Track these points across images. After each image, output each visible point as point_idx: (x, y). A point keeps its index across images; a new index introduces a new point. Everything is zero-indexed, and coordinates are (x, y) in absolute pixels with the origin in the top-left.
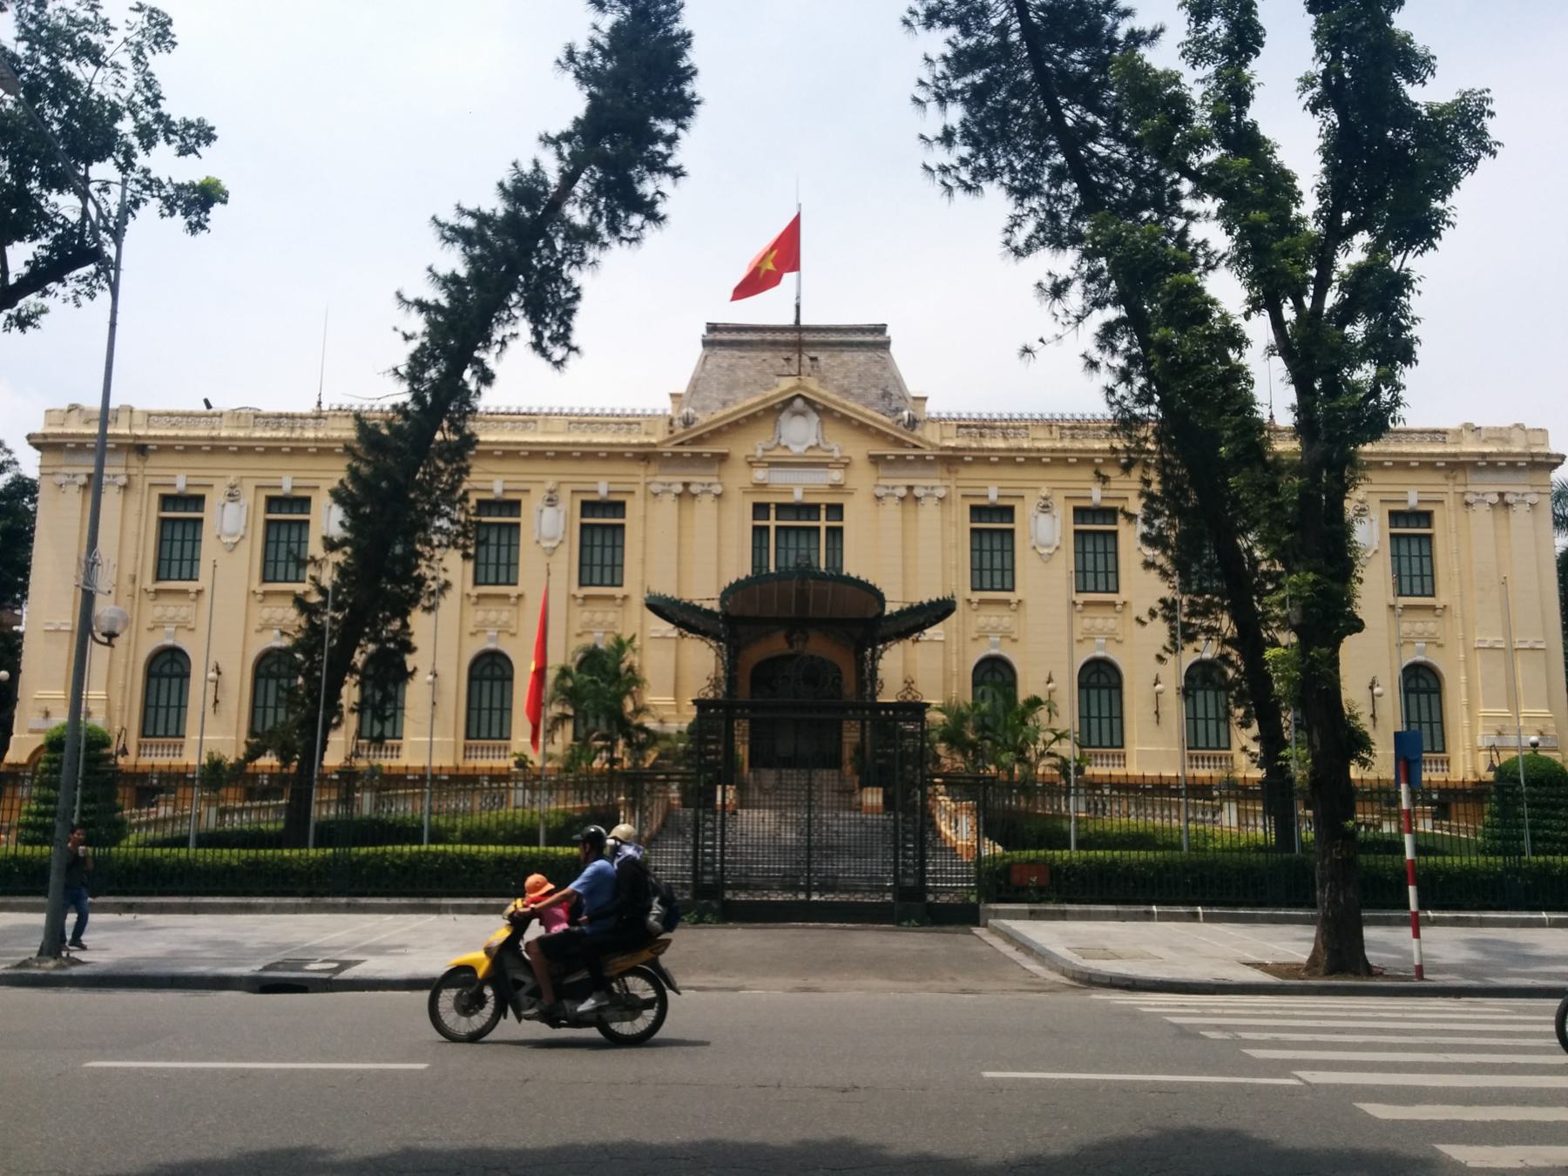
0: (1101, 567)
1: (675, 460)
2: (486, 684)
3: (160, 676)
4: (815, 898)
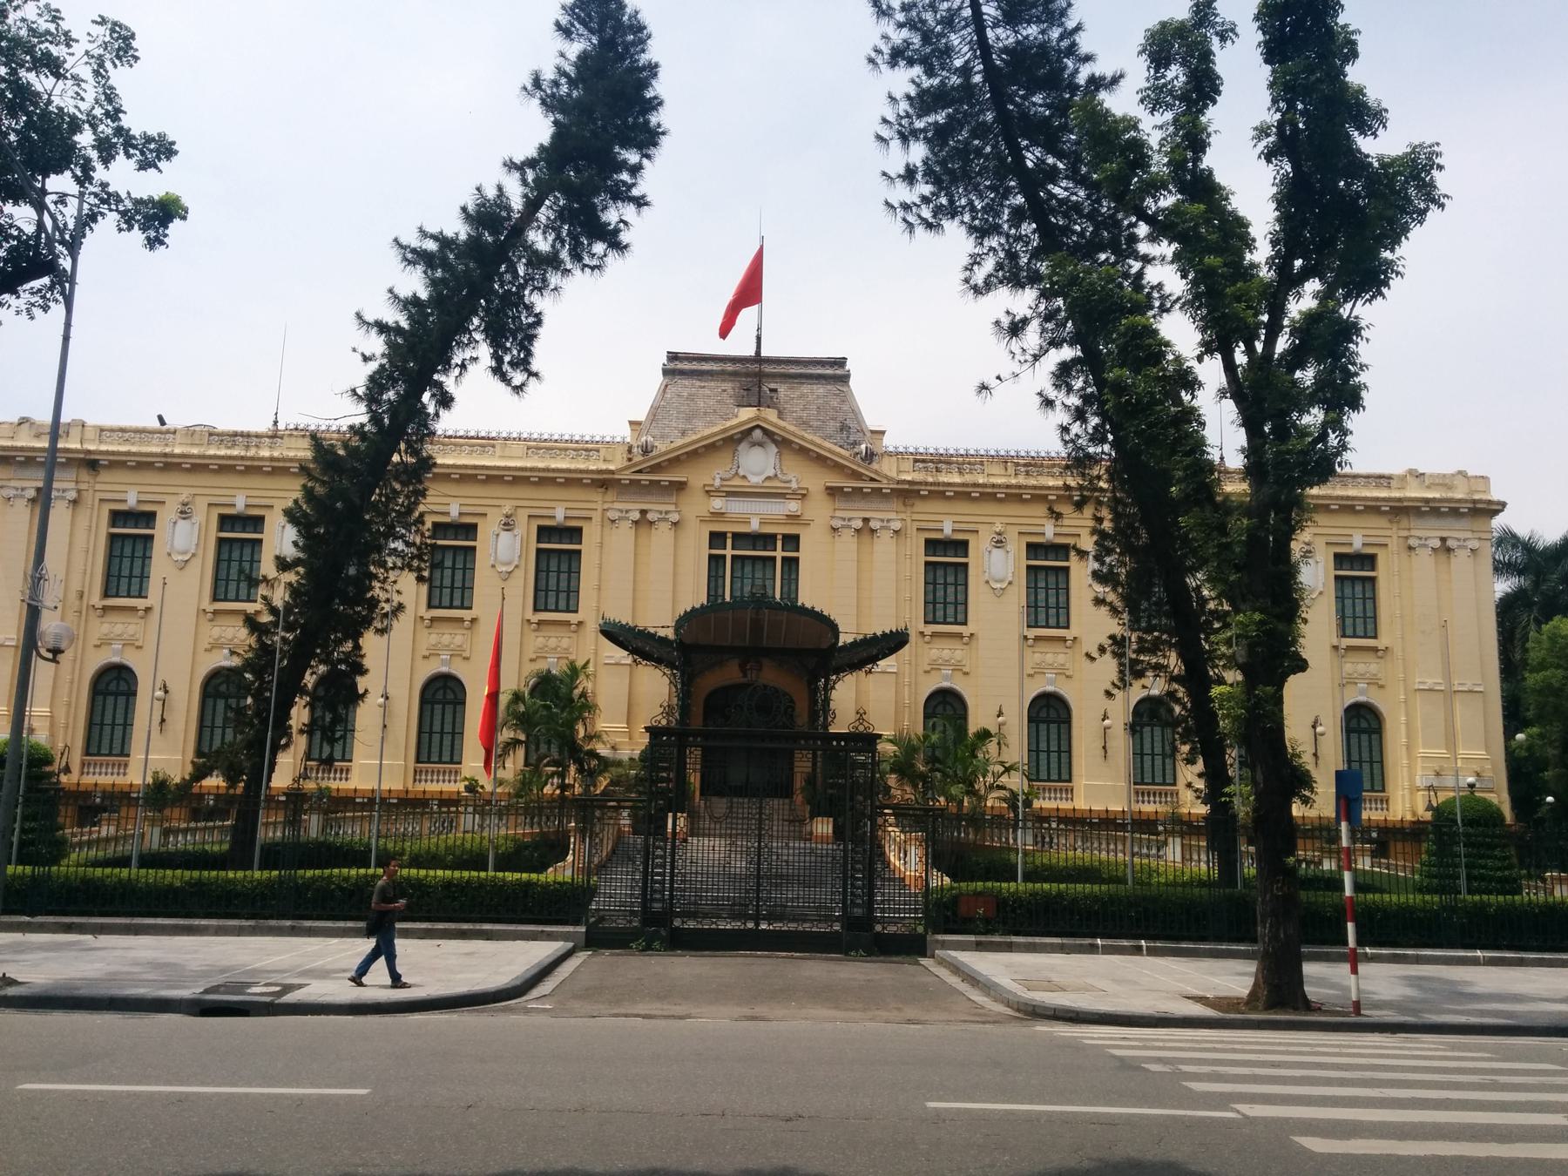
0: (1052, 601)
1: (634, 488)
2: (438, 707)
3: (106, 694)
4: (763, 926)
